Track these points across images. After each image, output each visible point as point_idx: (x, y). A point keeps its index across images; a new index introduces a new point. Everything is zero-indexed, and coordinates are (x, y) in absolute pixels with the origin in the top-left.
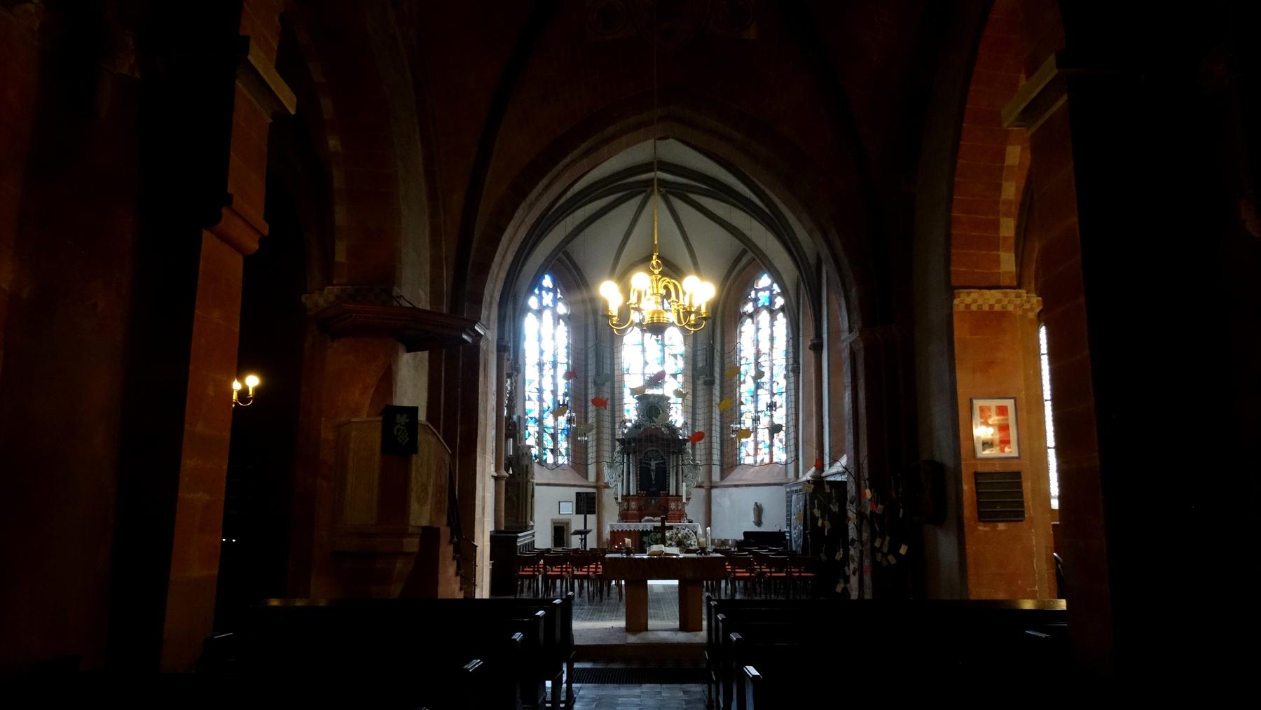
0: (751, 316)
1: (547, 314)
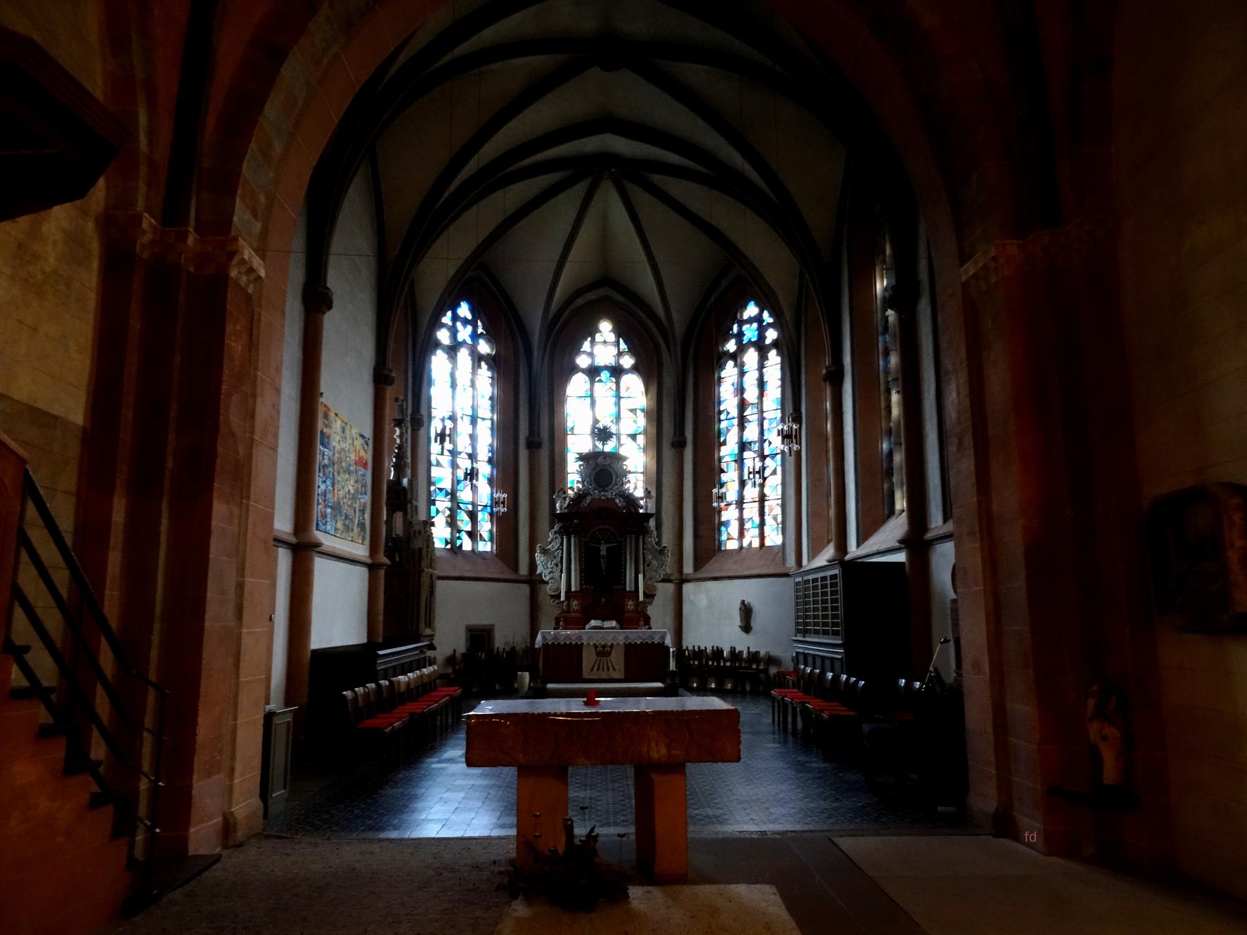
0: (734, 357)
1: (464, 355)
